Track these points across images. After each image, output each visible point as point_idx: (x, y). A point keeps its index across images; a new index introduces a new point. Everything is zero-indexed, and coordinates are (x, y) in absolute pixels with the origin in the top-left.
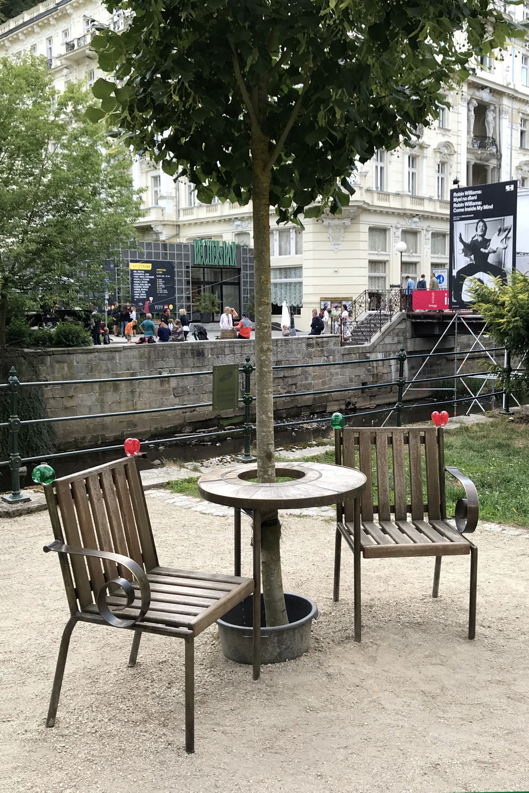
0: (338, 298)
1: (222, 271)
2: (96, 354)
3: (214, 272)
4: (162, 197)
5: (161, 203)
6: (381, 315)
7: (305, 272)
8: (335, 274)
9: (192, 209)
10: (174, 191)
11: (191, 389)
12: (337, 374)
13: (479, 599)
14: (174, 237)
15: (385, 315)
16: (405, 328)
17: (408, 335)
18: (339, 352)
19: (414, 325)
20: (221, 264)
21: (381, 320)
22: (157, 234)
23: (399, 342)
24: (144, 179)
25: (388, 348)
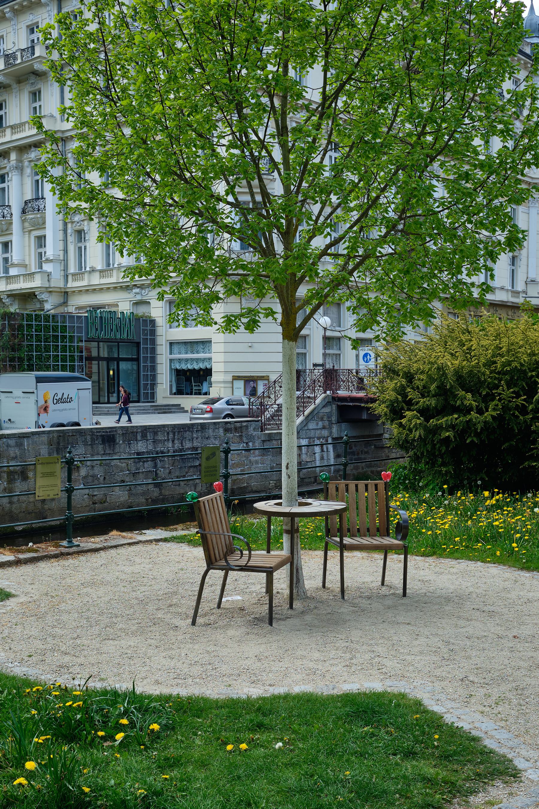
0: (253, 376)
1: (118, 345)
2: (5, 440)
3: (108, 346)
4: (48, 261)
5: (47, 267)
6: (304, 398)
7: (215, 347)
8: (250, 350)
9: (83, 273)
10: (61, 253)
11: (102, 478)
12: (257, 462)
13: (346, 574)
14: (61, 305)
15: (309, 397)
16: (331, 412)
17: (334, 419)
18: (259, 438)
19: (339, 408)
20: (118, 337)
21: (304, 403)
22: (42, 302)
23: (324, 428)
24: (27, 238)
25: (312, 434)
